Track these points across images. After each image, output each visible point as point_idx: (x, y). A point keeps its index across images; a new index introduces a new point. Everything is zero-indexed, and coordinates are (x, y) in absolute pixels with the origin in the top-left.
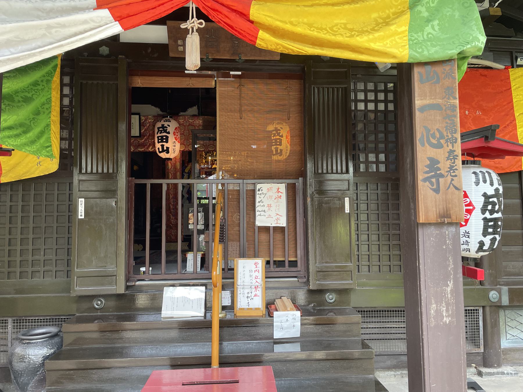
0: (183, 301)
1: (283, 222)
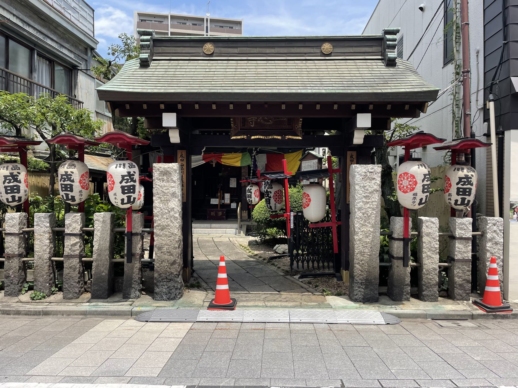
0: (214, 201)
1: (236, 187)
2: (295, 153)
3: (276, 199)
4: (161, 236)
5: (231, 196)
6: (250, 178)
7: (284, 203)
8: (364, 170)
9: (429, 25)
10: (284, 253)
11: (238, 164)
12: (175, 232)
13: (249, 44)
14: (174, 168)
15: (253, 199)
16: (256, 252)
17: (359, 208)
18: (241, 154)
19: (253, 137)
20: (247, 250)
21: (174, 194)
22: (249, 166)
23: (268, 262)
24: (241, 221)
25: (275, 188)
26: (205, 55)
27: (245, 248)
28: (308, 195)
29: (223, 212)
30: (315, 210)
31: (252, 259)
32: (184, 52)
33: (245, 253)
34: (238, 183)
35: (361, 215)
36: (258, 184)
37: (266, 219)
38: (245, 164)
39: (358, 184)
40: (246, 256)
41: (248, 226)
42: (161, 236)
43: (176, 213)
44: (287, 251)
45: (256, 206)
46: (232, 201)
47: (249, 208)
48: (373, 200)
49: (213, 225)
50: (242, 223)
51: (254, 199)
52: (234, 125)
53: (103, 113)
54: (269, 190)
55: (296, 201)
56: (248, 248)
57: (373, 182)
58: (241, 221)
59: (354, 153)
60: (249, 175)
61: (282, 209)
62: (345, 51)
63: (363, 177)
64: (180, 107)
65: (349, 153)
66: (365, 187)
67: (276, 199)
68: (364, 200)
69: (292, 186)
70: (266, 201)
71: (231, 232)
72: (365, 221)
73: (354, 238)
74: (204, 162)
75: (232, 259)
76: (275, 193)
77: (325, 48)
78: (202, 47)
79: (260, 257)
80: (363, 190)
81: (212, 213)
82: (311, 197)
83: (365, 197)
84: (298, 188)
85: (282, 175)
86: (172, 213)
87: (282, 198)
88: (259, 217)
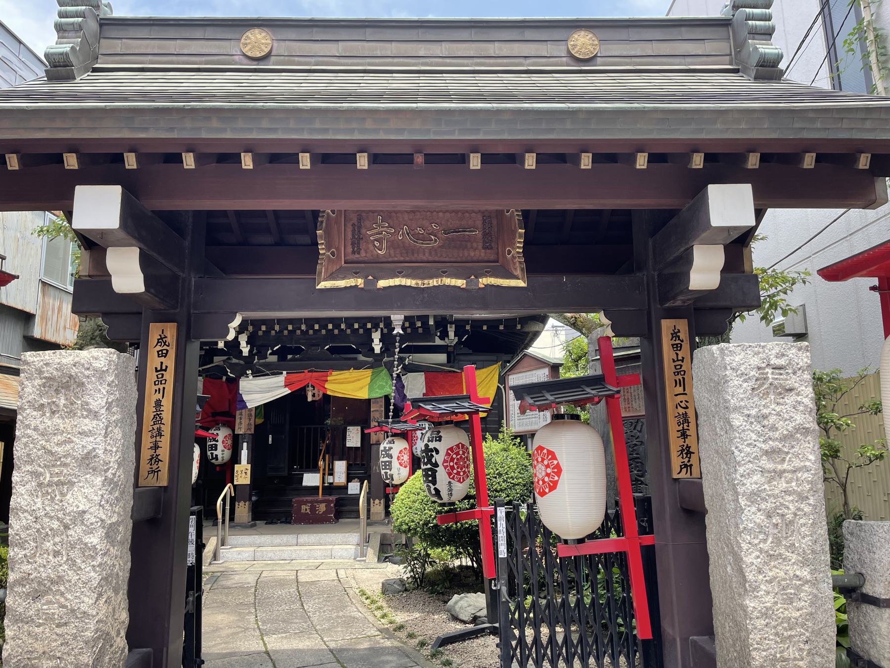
0: (311, 479)
1: (359, 445)
2: (484, 370)
3: (452, 468)
4: (29, 621)
5: (349, 467)
6: (387, 423)
7: (470, 480)
8: (755, 361)
9: (806, 37)
10: (475, 619)
11: (363, 395)
12: (84, 607)
13: (369, 33)
14: (96, 364)
15: (394, 471)
16: (400, 617)
17: (753, 493)
18: (369, 372)
19: (382, 283)
20: (380, 608)
21: (87, 460)
22: (387, 398)
23: (433, 656)
24: (368, 524)
25: (451, 438)
26: (245, 61)
27: (373, 602)
28: (550, 452)
29: (328, 502)
30: (574, 504)
31: (388, 643)
32: (186, 52)
33: (371, 619)
34: (365, 438)
35: (760, 518)
36: (404, 435)
37: (426, 523)
38: (378, 393)
39: (737, 409)
40: (373, 632)
41: (384, 537)
42: (29, 621)
43: (90, 532)
44: (484, 612)
45: (401, 489)
46: (349, 479)
47: (386, 492)
48: (797, 463)
49: (304, 538)
50: (371, 530)
51: (398, 471)
52: (328, 248)
53: (61, 286)
54: (432, 445)
55: (500, 475)
56: (382, 603)
57: (790, 399)
58: (368, 524)
59: (682, 325)
60: (387, 417)
61: (468, 497)
62: (633, 53)
63: (752, 383)
64: (131, 161)
65: (667, 325)
66: (765, 417)
67: (452, 468)
68: (765, 463)
69: (488, 435)
70: (426, 476)
71: (345, 554)
72: (777, 542)
73: (744, 608)
74: (287, 391)
75: (332, 645)
76: (448, 454)
77: (579, 43)
78: (240, 40)
79: (411, 636)
80: (758, 428)
81: (303, 507)
82: (563, 459)
83: (766, 453)
84: (503, 440)
85: (466, 404)
86: (75, 532)
87: (468, 467)
88: (407, 519)
